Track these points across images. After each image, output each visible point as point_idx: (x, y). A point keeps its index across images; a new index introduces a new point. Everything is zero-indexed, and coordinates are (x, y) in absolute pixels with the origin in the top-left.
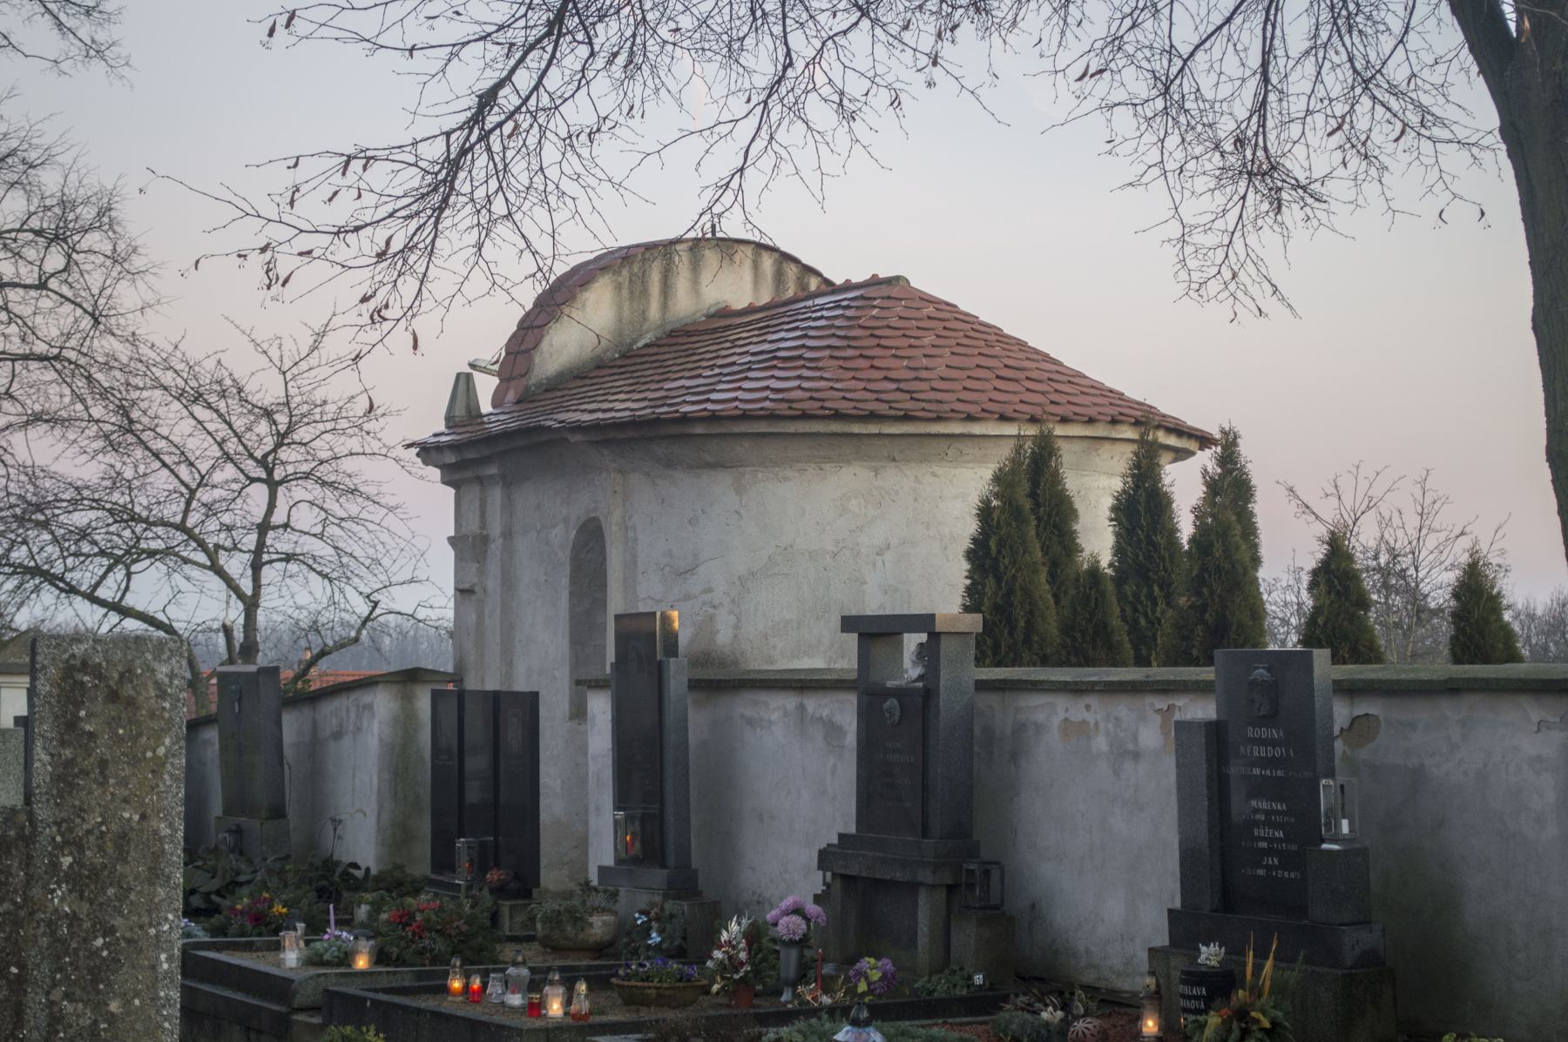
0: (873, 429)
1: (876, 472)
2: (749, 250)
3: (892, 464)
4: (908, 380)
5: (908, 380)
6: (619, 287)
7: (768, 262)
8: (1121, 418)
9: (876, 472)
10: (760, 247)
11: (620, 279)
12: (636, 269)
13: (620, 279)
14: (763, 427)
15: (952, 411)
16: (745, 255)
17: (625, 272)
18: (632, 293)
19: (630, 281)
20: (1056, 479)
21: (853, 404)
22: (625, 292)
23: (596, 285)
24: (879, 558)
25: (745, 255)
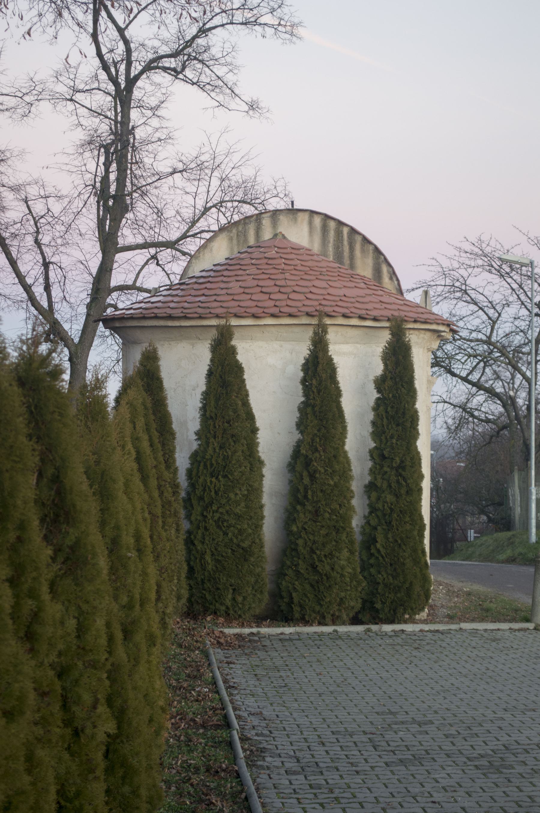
0: (170, 323)
1: (193, 345)
2: (306, 216)
3: (200, 341)
4: (228, 301)
5: (228, 301)
6: (231, 239)
7: (317, 221)
8: (406, 318)
9: (193, 345)
10: (313, 213)
11: (232, 235)
12: (240, 229)
13: (232, 235)
14: (162, 323)
15: (334, 311)
16: (304, 218)
17: (234, 231)
18: (238, 241)
19: (238, 235)
20: (233, 351)
21: (244, 309)
22: (235, 242)
23: (218, 238)
24: (193, 392)
25: (304, 218)
